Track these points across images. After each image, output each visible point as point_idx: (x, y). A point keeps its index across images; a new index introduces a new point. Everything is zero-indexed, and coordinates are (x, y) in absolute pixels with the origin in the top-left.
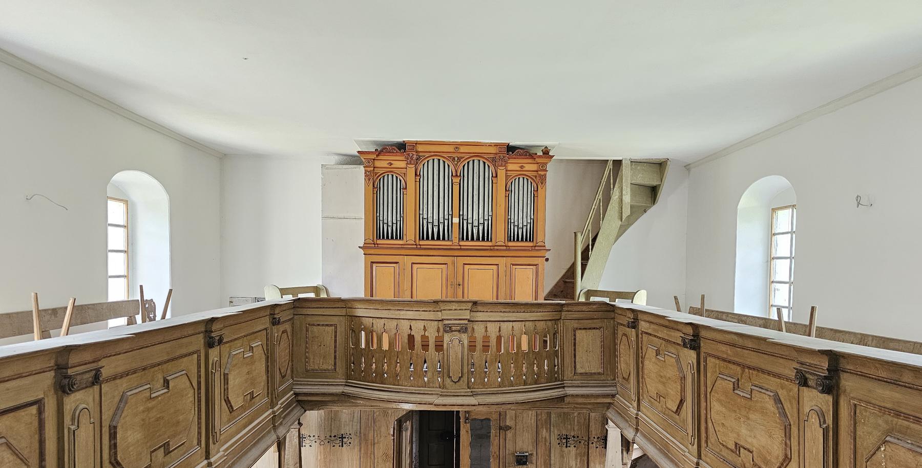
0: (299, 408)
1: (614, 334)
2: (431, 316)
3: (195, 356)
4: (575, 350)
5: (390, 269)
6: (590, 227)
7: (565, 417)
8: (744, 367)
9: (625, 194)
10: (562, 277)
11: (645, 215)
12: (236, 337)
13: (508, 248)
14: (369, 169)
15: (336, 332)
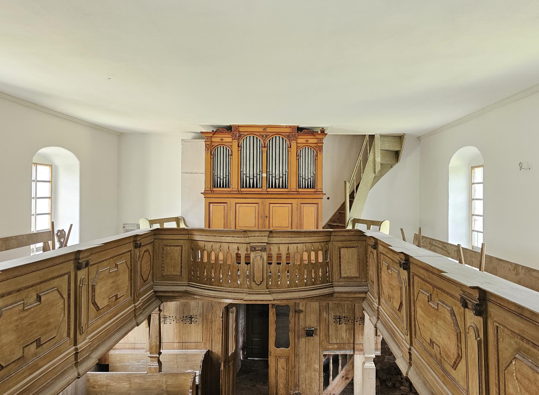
0: (157, 300)
1: (366, 251)
2: (242, 240)
3: (67, 276)
4: (340, 261)
5: (221, 206)
6: (354, 178)
7: (338, 305)
8: (434, 286)
10: (339, 210)
12: (103, 259)
13: (298, 193)
14: (208, 143)
15: (182, 250)
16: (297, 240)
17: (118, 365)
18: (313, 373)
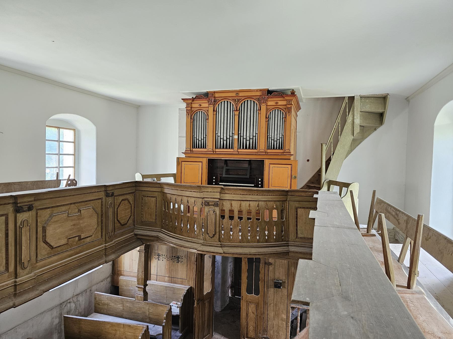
4: (297, 222)
6: (332, 140)
9: (357, 119)
11: (375, 132)
12: (58, 205)
16: (249, 197)
17: (125, 288)
18: (280, 322)
